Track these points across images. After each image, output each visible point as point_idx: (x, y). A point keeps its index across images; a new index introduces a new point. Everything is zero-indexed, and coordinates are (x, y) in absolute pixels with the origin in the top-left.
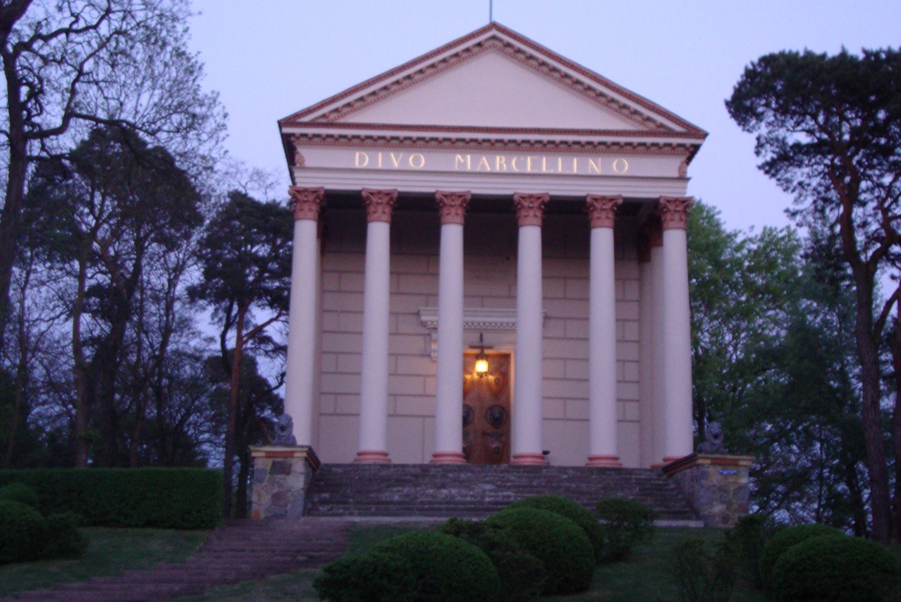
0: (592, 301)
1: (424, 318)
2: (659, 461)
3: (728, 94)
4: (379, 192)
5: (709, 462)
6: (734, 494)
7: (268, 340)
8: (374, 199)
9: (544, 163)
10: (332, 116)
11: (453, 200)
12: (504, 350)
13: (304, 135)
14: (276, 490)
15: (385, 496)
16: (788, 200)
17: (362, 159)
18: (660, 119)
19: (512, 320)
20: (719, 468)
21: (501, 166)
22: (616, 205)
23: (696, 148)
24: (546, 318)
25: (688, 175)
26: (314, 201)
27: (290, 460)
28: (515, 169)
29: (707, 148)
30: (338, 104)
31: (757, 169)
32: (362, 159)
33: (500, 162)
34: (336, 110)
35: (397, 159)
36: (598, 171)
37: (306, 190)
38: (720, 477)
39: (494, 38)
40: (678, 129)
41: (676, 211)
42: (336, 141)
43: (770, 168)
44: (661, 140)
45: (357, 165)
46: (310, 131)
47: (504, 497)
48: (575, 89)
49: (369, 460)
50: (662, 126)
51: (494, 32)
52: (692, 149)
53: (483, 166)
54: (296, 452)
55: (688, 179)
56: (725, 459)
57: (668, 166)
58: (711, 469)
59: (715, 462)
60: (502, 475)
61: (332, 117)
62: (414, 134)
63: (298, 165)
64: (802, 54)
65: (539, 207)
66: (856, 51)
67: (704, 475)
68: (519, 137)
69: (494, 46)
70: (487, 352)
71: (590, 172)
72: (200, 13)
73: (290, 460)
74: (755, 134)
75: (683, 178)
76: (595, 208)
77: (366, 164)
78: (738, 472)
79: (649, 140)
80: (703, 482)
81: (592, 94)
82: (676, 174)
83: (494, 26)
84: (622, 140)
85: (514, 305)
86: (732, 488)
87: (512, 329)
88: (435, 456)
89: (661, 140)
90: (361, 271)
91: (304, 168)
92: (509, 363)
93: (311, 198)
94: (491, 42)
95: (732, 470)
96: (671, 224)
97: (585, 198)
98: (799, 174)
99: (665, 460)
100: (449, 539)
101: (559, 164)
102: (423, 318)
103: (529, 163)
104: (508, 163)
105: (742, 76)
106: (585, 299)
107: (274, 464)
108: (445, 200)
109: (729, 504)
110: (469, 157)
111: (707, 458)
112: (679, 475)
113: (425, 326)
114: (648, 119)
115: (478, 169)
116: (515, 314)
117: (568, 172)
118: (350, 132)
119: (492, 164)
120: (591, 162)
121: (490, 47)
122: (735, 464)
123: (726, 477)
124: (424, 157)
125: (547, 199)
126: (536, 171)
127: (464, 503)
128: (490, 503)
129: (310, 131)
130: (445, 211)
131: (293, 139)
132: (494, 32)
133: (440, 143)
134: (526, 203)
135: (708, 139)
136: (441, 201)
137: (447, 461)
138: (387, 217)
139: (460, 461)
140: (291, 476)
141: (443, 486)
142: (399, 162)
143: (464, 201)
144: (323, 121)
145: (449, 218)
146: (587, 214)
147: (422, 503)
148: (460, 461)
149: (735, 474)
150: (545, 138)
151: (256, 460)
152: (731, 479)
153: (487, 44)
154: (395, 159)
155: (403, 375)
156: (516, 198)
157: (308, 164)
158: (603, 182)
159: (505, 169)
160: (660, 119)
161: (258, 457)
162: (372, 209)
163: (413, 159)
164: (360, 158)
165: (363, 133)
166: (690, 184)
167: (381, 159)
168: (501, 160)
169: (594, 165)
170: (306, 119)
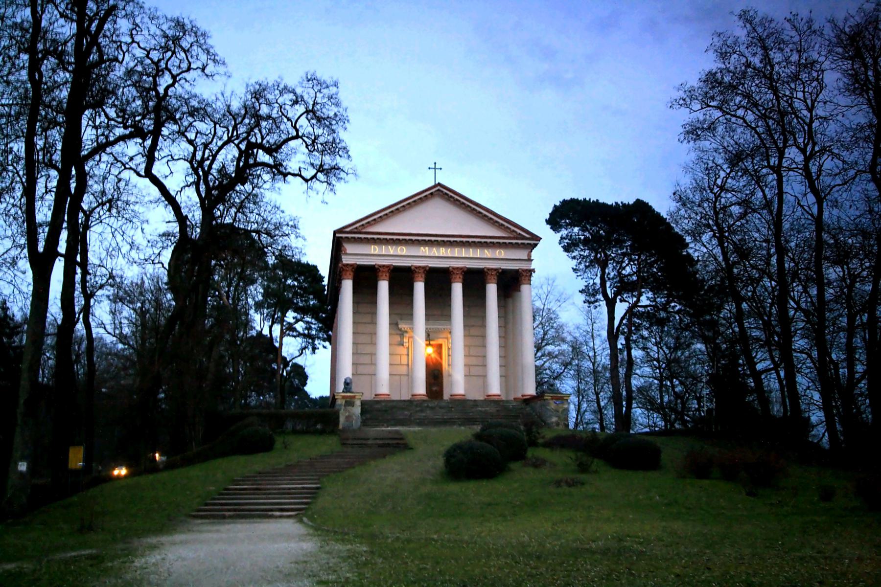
0: (414, 315)
2: (519, 396)
9: (463, 252)
10: (360, 228)
12: (440, 341)
13: (347, 238)
14: (347, 414)
17: (375, 249)
18: (519, 231)
22: (463, 271)
23: (536, 245)
27: (353, 400)
29: (541, 244)
30: (364, 222)
32: (375, 249)
33: (443, 251)
36: (489, 256)
37: (347, 265)
39: (439, 190)
40: (527, 236)
44: (520, 242)
46: (350, 236)
51: (438, 188)
57: (522, 254)
58: (552, 402)
59: (553, 398)
62: (407, 238)
66: (601, 201)
67: (548, 404)
68: (452, 239)
70: (432, 343)
71: (485, 256)
73: (353, 400)
75: (530, 260)
77: (376, 252)
79: (514, 241)
83: (439, 184)
84: (501, 241)
86: (561, 410)
88: (413, 395)
89: (520, 242)
91: (346, 254)
93: (460, 272)
96: (345, 277)
97: (483, 269)
99: (522, 396)
100: (479, 443)
101: (471, 253)
103: (456, 252)
107: (346, 402)
109: (559, 417)
110: (427, 248)
112: (533, 404)
114: (514, 231)
115: (432, 255)
117: (460, 256)
120: (486, 251)
125: (465, 269)
129: (350, 236)
130: (454, 276)
132: (438, 188)
133: (412, 242)
134: (455, 271)
137: (418, 398)
138: (461, 280)
139: (426, 398)
143: (463, 271)
144: (356, 230)
148: (426, 398)
152: (560, 406)
153: (401, 209)
154: (391, 250)
157: (348, 252)
159: (445, 255)
160: (519, 231)
162: (380, 274)
164: (374, 249)
165: (376, 237)
166: (533, 262)
167: (384, 250)
169: (487, 253)
170: (348, 230)
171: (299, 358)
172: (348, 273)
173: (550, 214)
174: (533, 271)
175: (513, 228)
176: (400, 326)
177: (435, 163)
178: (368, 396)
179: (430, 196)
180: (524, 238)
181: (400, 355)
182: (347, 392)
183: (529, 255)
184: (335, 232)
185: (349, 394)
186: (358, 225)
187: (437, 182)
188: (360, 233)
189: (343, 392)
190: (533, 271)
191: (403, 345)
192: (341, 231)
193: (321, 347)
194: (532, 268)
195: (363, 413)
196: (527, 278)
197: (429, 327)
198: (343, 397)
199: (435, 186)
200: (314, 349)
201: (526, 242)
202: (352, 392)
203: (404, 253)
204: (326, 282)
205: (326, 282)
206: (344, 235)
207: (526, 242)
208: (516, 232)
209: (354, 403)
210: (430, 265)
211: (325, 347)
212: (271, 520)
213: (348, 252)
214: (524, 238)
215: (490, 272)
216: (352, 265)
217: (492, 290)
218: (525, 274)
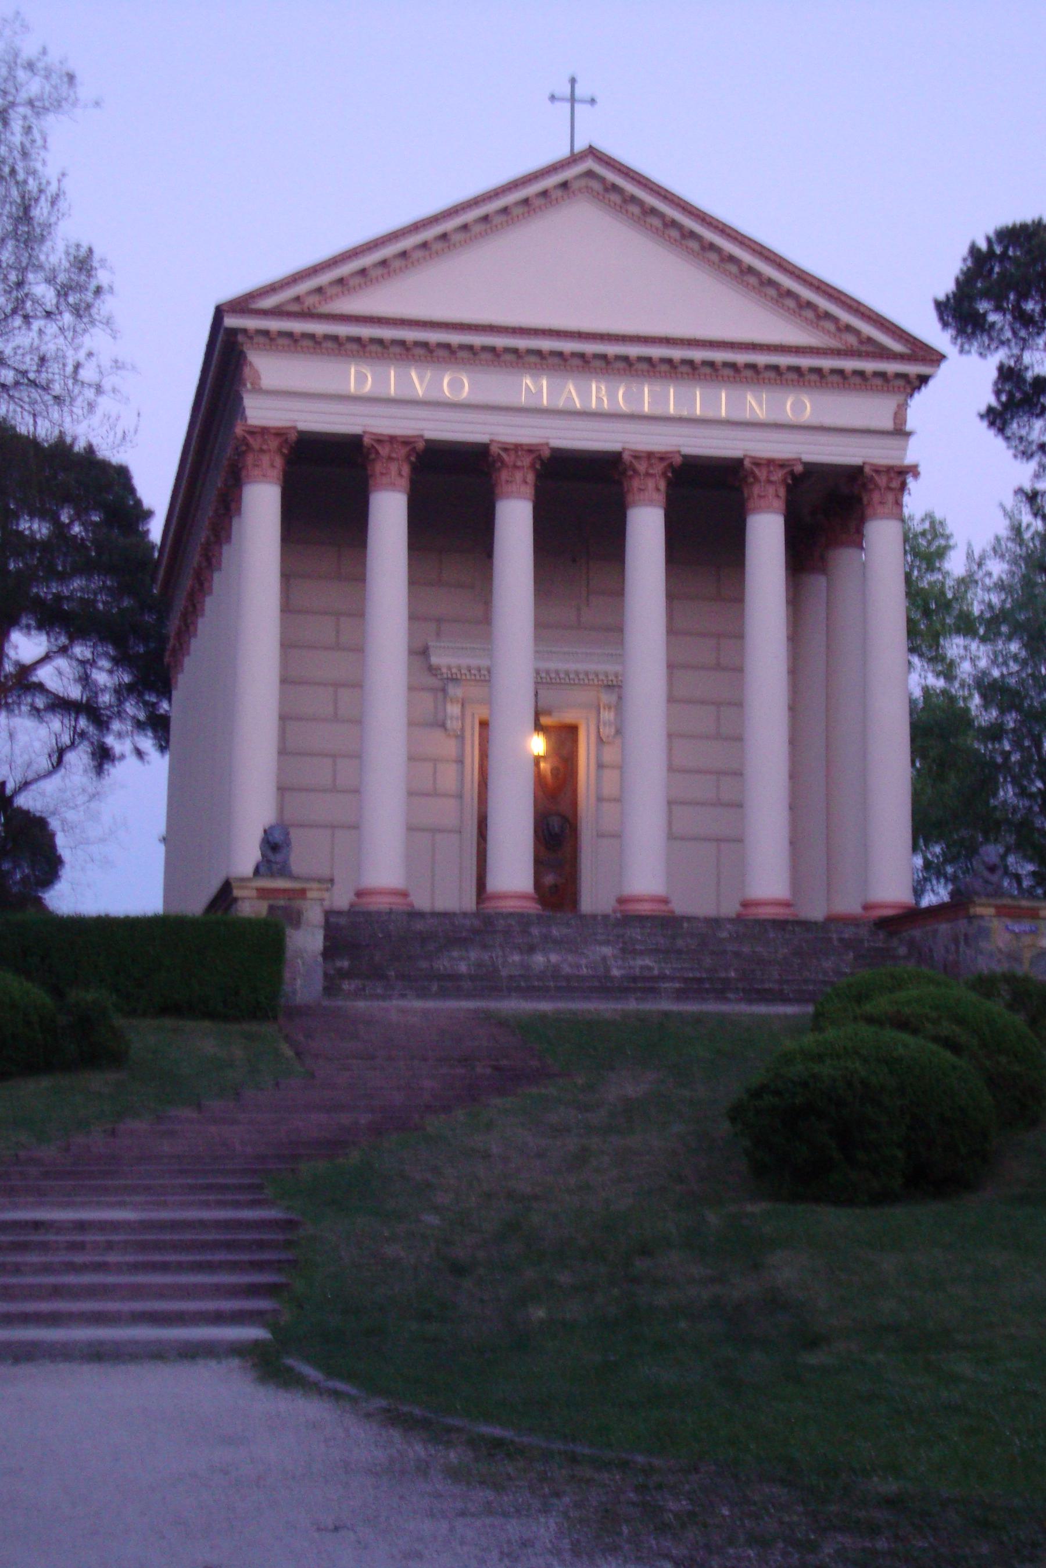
1: (434, 660)
3: (945, 286)
7: (40, 687)
8: (384, 451)
12: (569, 717)
15: (442, 964)
17: (361, 379)
18: (867, 329)
19: (483, 663)
20: (1009, 922)
21: (599, 399)
25: (909, 426)
27: (298, 903)
28: (622, 405)
30: (323, 279)
31: (978, 419)
32: (361, 379)
34: (320, 290)
35: (421, 379)
37: (264, 431)
38: (1007, 936)
39: (590, 174)
40: (897, 347)
41: (769, 482)
42: (315, 344)
44: (869, 366)
46: (274, 325)
47: (642, 967)
49: (380, 904)
50: (870, 340)
51: (590, 164)
53: (570, 398)
54: (311, 889)
55: (908, 434)
56: (1019, 907)
58: (996, 924)
59: (1003, 912)
61: (310, 301)
63: (249, 386)
67: (985, 933)
68: (634, 351)
69: (589, 189)
71: (747, 416)
72: (97, 104)
73: (298, 903)
75: (900, 432)
77: (368, 387)
78: (1037, 928)
80: (983, 944)
81: (753, 280)
82: (888, 424)
83: (592, 152)
85: (621, 642)
86: (1027, 955)
87: (485, 677)
89: (869, 366)
90: (618, 591)
91: (258, 390)
92: (575, 741)
94: (583, 182)
95: (1025, 925)
96: (256, 472)
99: (866, 907)
104: (612, 396)
105: (965, 260)
106: (359, 613)
108: (504, 455)
111: (989, 905)
113: (436, 675)
114: (849, 328)
115: (561, 404)
116: (620, 657)
117: (710, 414)
118: (342, 330)
119: (585, 395)
120: (750, 398)
121: (580, 190)
123: (1017, 936)
124: (811, 401)
125: (678, 460)
126: (658, 411)
129: (274, 325)
131: (241, 338)
132: (590, 164)
135: (944, 366)
136: (500, 457)
139: (532, 908)
141: (531, 949)
142: (425, 385)
144: (295, 308)
146: (620, 483)
150: (741, 358)
151: (240, 903)
152: (1027, 940)
153: (576, 185)
156: (494, 449)
158: (394, 411)
160: (867, 329)
161: (244, 899)
162: (378, 467)
163: (793, 405)
166: (913, 441)
168: (598, 389)
171: (50, 785)
172: (265, 459)
173: (958, 282)
174: (913, 470)
175: (846, 317)
176: (434, 660)
177: (573, 81)
178: (342, 899)
179: (559, 193)
180: (885, 353)
181: (435, 761)
182: (272, 875)
183: (900, 416)
184: (219, 313)
185: (281, 883)
186: (301, 288)
187: (580, 146)
188: (309, 315)
189: (257, 872)
190: (913, 470)
191: (443, 726)
192: (241, 305)
193: (132, 760)
194: (909, 460)
195: (329, 952)
196: (890, 497)
198: (263, 893)
199: (574, 159)
200: (103, 756)
201: (891, 367)
202: (291, 877)
203: (465, 393)
204: (156, 529)
205: (156, 529)
206: (251, 323)
207: (891, 367)
208: (857, 332)
209: (299, 913)
211: (139, 753)
212: (25, 1369)
214: (885, 353)
215: (762, 474)
216: (280, 433)
218: (882, 481)
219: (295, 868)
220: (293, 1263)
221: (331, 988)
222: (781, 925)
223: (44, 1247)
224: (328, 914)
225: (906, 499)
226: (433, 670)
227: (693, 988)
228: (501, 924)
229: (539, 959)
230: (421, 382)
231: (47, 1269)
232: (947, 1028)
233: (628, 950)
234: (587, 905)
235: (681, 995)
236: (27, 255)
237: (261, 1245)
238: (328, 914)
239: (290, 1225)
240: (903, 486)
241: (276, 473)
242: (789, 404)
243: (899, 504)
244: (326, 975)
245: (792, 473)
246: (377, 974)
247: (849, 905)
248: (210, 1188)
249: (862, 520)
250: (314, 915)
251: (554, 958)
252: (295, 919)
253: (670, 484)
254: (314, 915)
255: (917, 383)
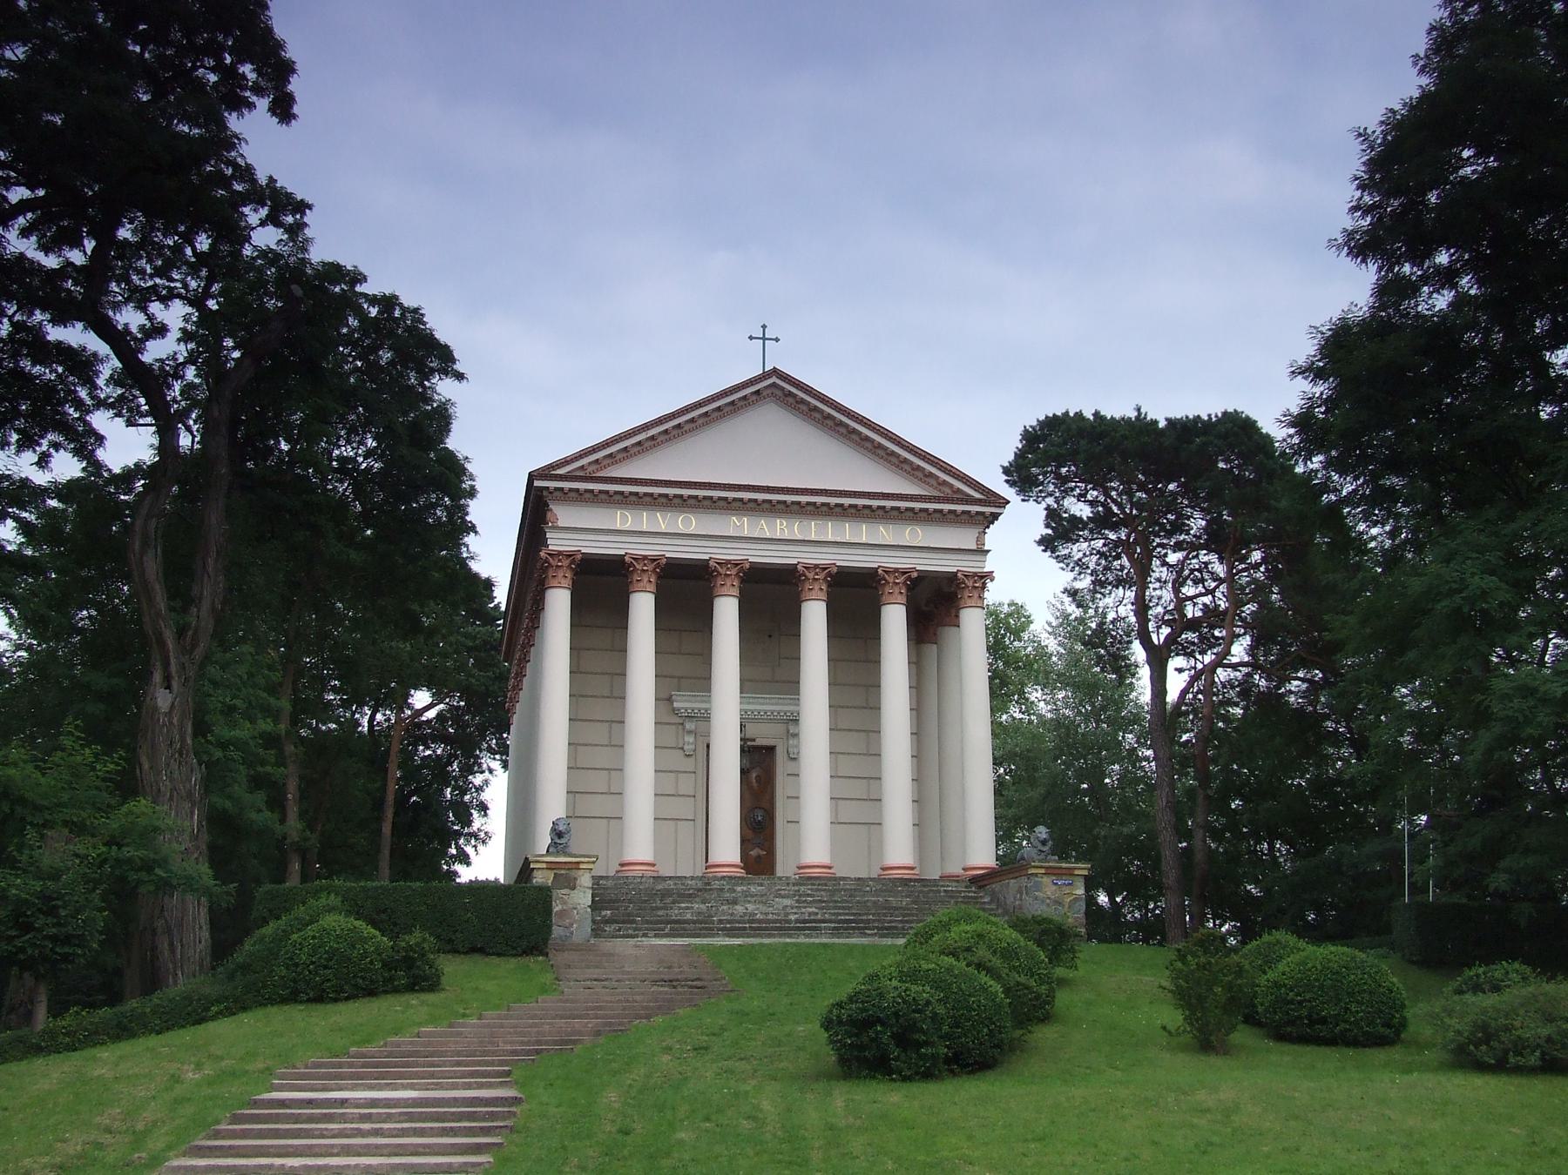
4: (645, 557)
5: (1043, 871)
6: (1069, 907)
9: (830, 530)
11: (560, 561)
15: (674, 913)
16: (1065, 578)
19: (704, 705)
22: (829, 574)
23: (995, 517)
24: (741, 703)
26: (569, 567)
27: (573, 873)
37: (560, 553)
38: (1054, 888)
39: (774, 385)
40: (977, 496)
43: (1047, 543)
44: (959, 508)
45: (618, 526)
46: (566, 485)
48: (863, 447)
49: (637, 871)
51: (774, 379)
52: (991, 519)
57: (962, 537)
60: (797, 888)
64: (1089, 415)
65: (569, 567)
68: (847, 501)
73: (573, 873)
74: (1044, 505)
76: (635, 569)
79: (946, 507)
83: (775, 371)
89: (959, 508)
93: (566, 562)
94: (769, 391)
98: (1078, 549)
102: (675, 705)
111: (1041, 867)
114: (945, 483)
116: (708, 699)
122: (1070, 873)
127: (768, 921)
128: (797, 921)
129: (566, 485)
131: (545, 493)
132: (774, 379)
139: (741, 873)
140: (575, 891)
141: (735, 902)
145: (725, 590)
147: (720, 921)
149: (1069, 884)
154: (662, 521)
155: (671, 772)
164: (622, 519)
167: (646, 520)
168: (781, 524)
169: (885, 533)
176: (675, 705)
178: (603, 868)
182: (558, 853)
183: (980, 540)
184: (532, 477)
192: (545, 473)
195: (595, 906)
197: (746, 707)
198: (551, 866)
199: (765, 375)
208: (951, 486)
210: (752, 559)
213: (560, 524)
217: (894, 619)
219: (573, 849)
220: (511, 1129)
221: (597, 931)
222: (905, 882)
223: (343, 1118)
224: (597, 880)
225: (986, 594)
226: (675, 711)
227: (842, 928)
228: (716, 885)
229: (739, 909)
230: (664, 523)
231: (342, 1134)
232: (982, 953)
233: (801, 899)
234: (780, 872)
235: (836, 932)
236: (1158, 550)
237: (493, 1116)
238: (597, 880)
239: (516, 1101)
240: (984, 587)
241: (567, 582)
242: (907, 532)
243: (981, 598)
244: (594, 921)
245: (909, 578)
246: (628, 920)
247: (955, 869)
248: (472, 1074)
249: (958, 609)
250: (585, 880)
251: (751, 907)
252: (572, 885)
253: (829, 585)
254: (585, 880)
255: (991, 519)
